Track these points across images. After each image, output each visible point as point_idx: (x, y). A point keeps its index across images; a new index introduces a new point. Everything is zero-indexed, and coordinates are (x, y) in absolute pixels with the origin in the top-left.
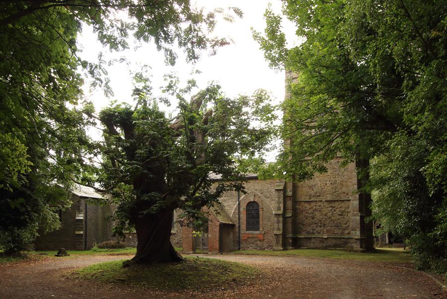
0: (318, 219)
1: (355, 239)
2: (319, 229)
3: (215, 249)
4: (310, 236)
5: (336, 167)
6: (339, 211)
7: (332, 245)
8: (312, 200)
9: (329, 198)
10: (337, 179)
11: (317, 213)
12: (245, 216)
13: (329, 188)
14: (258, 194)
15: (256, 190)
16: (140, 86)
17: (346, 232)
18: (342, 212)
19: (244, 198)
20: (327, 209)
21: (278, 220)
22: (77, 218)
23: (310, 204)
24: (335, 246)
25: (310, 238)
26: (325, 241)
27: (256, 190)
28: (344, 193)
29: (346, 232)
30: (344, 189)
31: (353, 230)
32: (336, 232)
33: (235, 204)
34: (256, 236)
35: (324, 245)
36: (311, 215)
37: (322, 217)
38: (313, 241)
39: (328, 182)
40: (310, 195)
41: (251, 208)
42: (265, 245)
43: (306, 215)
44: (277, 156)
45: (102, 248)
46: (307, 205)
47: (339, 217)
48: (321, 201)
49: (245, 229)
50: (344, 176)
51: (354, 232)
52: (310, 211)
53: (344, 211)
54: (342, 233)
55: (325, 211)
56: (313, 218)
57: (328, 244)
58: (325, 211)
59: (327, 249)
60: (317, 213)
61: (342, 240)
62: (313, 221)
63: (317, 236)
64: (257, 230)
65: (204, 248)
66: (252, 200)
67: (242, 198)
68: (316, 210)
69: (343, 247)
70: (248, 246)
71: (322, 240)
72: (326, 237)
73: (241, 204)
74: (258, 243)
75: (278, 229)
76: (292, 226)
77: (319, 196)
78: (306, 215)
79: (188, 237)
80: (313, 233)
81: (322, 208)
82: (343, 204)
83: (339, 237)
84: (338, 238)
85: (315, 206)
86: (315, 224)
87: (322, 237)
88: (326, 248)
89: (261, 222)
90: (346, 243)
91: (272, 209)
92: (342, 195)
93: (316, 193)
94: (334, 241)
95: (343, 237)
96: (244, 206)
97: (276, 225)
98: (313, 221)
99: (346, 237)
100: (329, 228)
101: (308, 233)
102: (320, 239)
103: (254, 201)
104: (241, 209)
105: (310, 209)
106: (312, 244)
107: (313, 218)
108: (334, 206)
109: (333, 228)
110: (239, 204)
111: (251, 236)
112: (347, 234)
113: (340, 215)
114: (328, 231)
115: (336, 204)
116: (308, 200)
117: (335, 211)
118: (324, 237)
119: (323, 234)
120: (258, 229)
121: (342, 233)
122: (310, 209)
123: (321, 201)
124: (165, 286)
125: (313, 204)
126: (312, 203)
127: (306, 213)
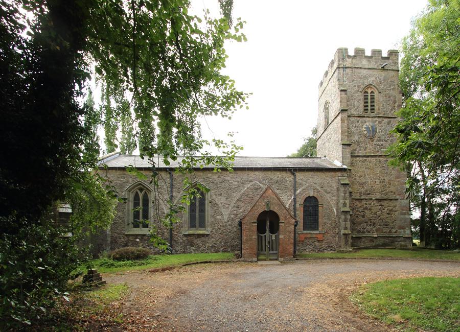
0: (368, 218)
1: (404, 238)
2: (369, 227)
3: (289, 254)
4: (361, 236)
5: (384, 165)
6: (387, 210)
7: (381, 244)
8: (362, 198)
9: (378, 197)
10: (385, 178)
11: (367, 212)
12: (303, 213)
13: (378, 186)
14: (318, 188)
15: (315, 183)
16: (238, 27)
17: (394, 230)
18: (391, 210)
19: (300, 192)
20: (376, 208)
21: (345, 218)
22: (61, 210)
23: (360, 202)
24: (384, 246)
25: (360, 238)
26: (374, 239)
27: (315, 183)
28: (392, 192)
29: (394, 230)
30: (392, 189)
31: (400, 229)
32: (384, 231)
33: (289, 199)
34: (314, 236)
35: (374, 244)
36: (362, 214)
37: (371, 216)
38: (363, 240)
39: (377, 180)
40: (361, 193)
41: (308, 204)
42: (324, 246)
43: (357, 213)
44: (84, 87)
45: (119, 259)
46: (357, 203)
47: (388, 216)
48: (371, 199)
49: (302, 228)
50: (392, 175)
51: (402, 230)
52: (360, 209)
53: (392, 210)
54: (390, 232)
55: (375, 209)
56: (363, 216)
57: (377, 243)
58: (375, 209)
59: (378, 248)
60: (367, 212)
61: (390, 239)
62: (363, 219)
63: (368, 235)
64: (316, 230)
65: (272, 252)
66: (311, 195)
67: (298, 192)
68: (366, 208)
69: (390, 246)
70: (305, 248)
71: (372, 239)
72: (376, 236)
73: (297, 199)
74: (317, 244)
75: (346, 228)
76: (318, 218)
77: (369, 194)
78: (357, 213)
79: (251, 240)
80: (363, 232)
81: (372, 207)
82: (390, 203)
83: (387, 235)
84: (386, 237)
85: (366, 204)
86: (365, 222)
87: (372, 236)
88: (376, 247)
89: (320, 220)
90: (393, 242)
91: (333, 205)
92: (390, 194)
93: (367, 190)
94: (382, 241)
95: (391, 235)
96: (300, 201)
97: (343, 224)
98: (363, 219)
99: (394, 236)
100: (378, 227)
101: (359, 232)
102: (371, 238)
103: (313, 197)
104: (297, 205)
105: (361, 207)
106: (362, 244)
107: (363, 216)
108: (383, 204)
109: (382, 227)
110: (295, 199)
111: (309, 236)
112: (395, 232)
113: (388, 214)
114: (377, 230)
115: (385, 203)
116: (359, 198)
117: (384, 209)
118: (375, 236)
119: (373, 233)
120: (317, 229)
121: (390, 232)
122: (361, 207)
123: (371, 199)
124: (155, 311)
125: (364, 202)
126: (363, 201)
127: (357, 211)
